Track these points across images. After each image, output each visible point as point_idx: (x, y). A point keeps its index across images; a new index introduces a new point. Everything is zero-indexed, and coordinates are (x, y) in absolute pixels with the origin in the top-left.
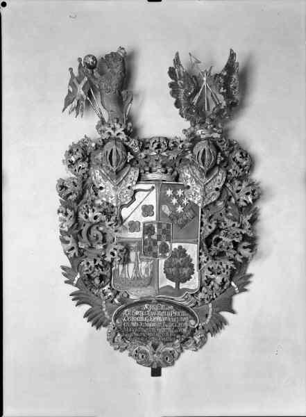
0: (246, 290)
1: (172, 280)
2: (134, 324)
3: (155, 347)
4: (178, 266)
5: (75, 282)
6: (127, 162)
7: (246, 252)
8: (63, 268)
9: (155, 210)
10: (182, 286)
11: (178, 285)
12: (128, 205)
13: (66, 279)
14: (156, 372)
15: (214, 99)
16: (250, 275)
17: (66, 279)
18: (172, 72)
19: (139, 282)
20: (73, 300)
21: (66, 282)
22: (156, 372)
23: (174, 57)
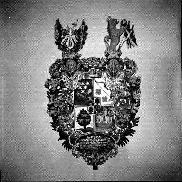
0: (137, 125)
1: (82, 125)
2: (105, 145)
3: (96, 156)
4: (84, 118)
5: (133, 125)
6: (77, 69)
7: (52, 112)
8: (51, 123)
9: (95, 92)
10: (87, 127)
11: (85, 127)
12: (105, 86)
13: (53, 128)
14: (95, 168)
15: (70, 40)
16: (138, 118)
17: (53, 128)
18: (108, 21)
19: (103, 125)
20: (134, 133)
21: (53, 130)
22: (95, 168)
23: (55, 23)
